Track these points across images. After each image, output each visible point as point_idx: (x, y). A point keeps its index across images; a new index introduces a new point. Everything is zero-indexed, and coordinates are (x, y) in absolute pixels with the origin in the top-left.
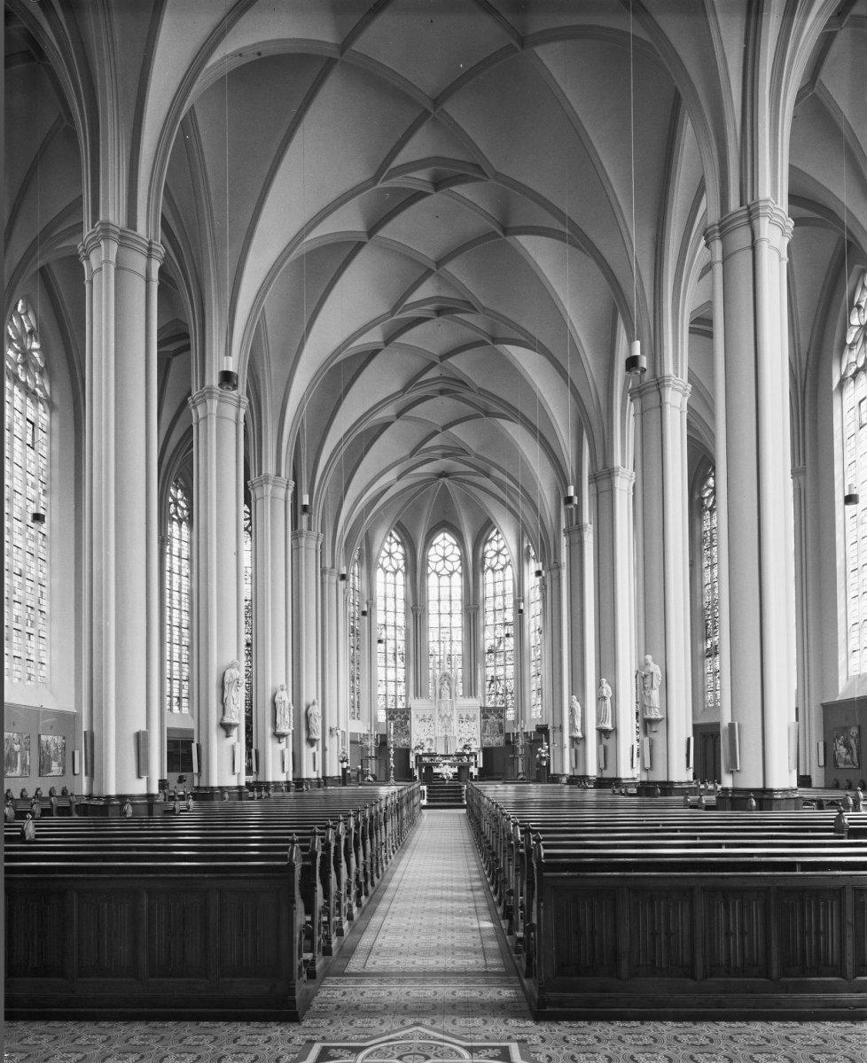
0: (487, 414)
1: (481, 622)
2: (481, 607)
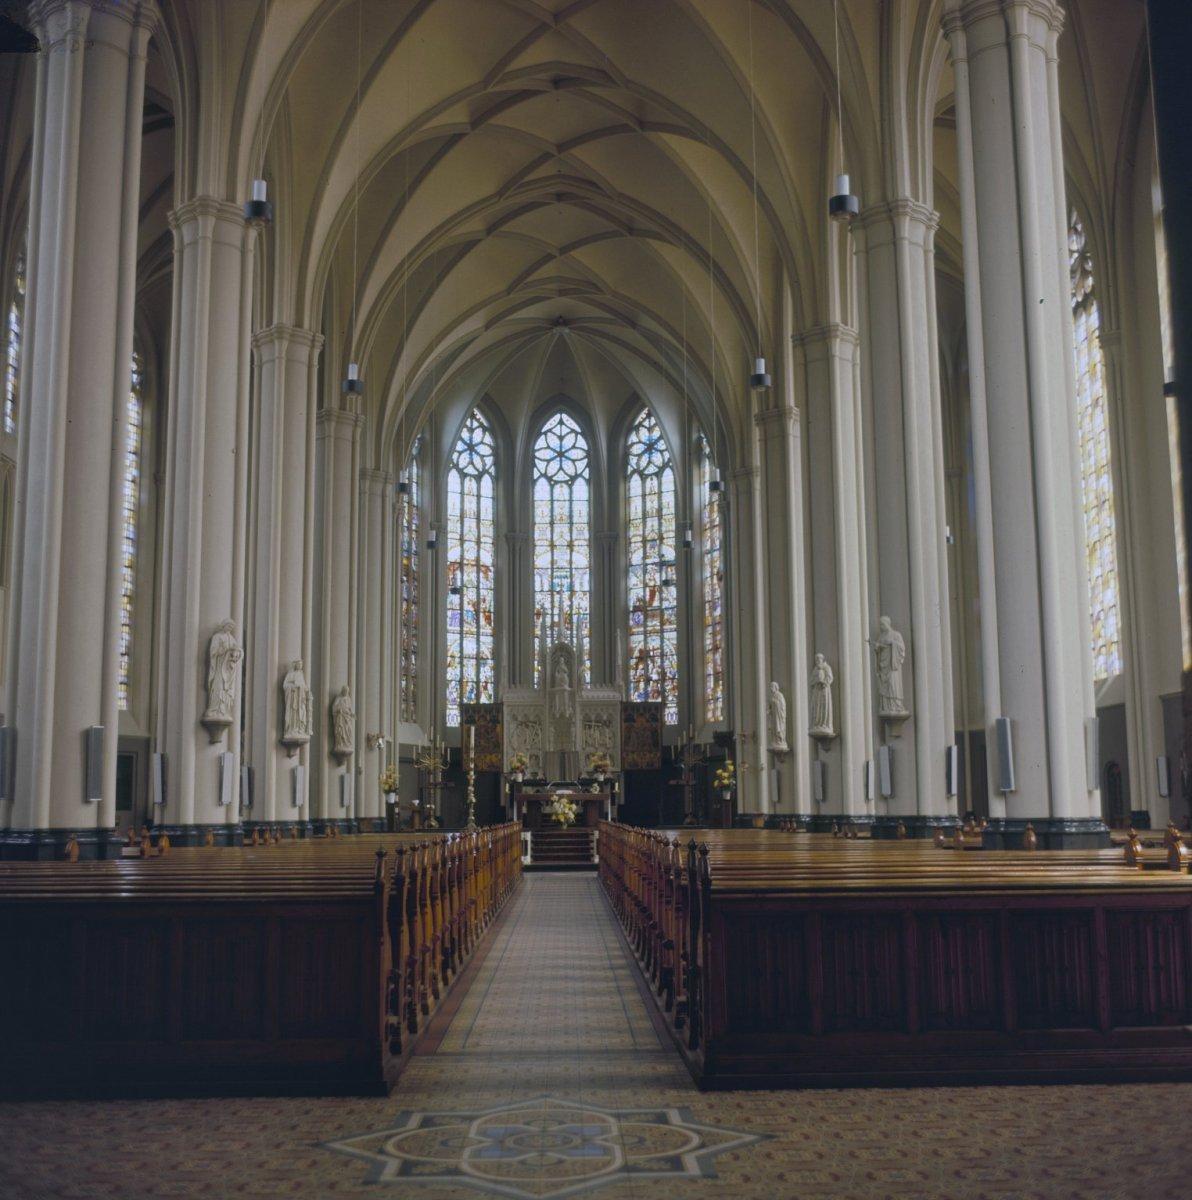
0: (631, 231)
1: (623, 559)
2: (622, 534)
